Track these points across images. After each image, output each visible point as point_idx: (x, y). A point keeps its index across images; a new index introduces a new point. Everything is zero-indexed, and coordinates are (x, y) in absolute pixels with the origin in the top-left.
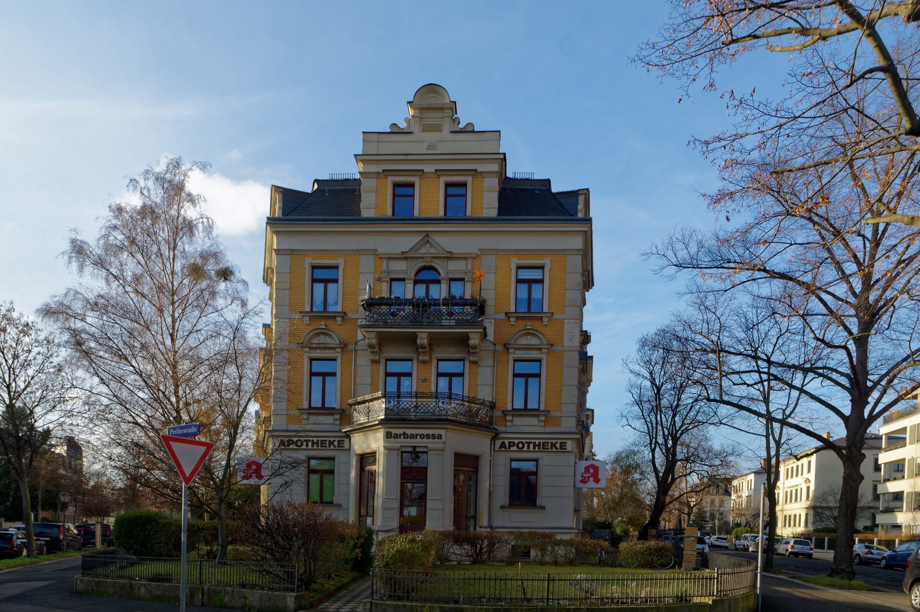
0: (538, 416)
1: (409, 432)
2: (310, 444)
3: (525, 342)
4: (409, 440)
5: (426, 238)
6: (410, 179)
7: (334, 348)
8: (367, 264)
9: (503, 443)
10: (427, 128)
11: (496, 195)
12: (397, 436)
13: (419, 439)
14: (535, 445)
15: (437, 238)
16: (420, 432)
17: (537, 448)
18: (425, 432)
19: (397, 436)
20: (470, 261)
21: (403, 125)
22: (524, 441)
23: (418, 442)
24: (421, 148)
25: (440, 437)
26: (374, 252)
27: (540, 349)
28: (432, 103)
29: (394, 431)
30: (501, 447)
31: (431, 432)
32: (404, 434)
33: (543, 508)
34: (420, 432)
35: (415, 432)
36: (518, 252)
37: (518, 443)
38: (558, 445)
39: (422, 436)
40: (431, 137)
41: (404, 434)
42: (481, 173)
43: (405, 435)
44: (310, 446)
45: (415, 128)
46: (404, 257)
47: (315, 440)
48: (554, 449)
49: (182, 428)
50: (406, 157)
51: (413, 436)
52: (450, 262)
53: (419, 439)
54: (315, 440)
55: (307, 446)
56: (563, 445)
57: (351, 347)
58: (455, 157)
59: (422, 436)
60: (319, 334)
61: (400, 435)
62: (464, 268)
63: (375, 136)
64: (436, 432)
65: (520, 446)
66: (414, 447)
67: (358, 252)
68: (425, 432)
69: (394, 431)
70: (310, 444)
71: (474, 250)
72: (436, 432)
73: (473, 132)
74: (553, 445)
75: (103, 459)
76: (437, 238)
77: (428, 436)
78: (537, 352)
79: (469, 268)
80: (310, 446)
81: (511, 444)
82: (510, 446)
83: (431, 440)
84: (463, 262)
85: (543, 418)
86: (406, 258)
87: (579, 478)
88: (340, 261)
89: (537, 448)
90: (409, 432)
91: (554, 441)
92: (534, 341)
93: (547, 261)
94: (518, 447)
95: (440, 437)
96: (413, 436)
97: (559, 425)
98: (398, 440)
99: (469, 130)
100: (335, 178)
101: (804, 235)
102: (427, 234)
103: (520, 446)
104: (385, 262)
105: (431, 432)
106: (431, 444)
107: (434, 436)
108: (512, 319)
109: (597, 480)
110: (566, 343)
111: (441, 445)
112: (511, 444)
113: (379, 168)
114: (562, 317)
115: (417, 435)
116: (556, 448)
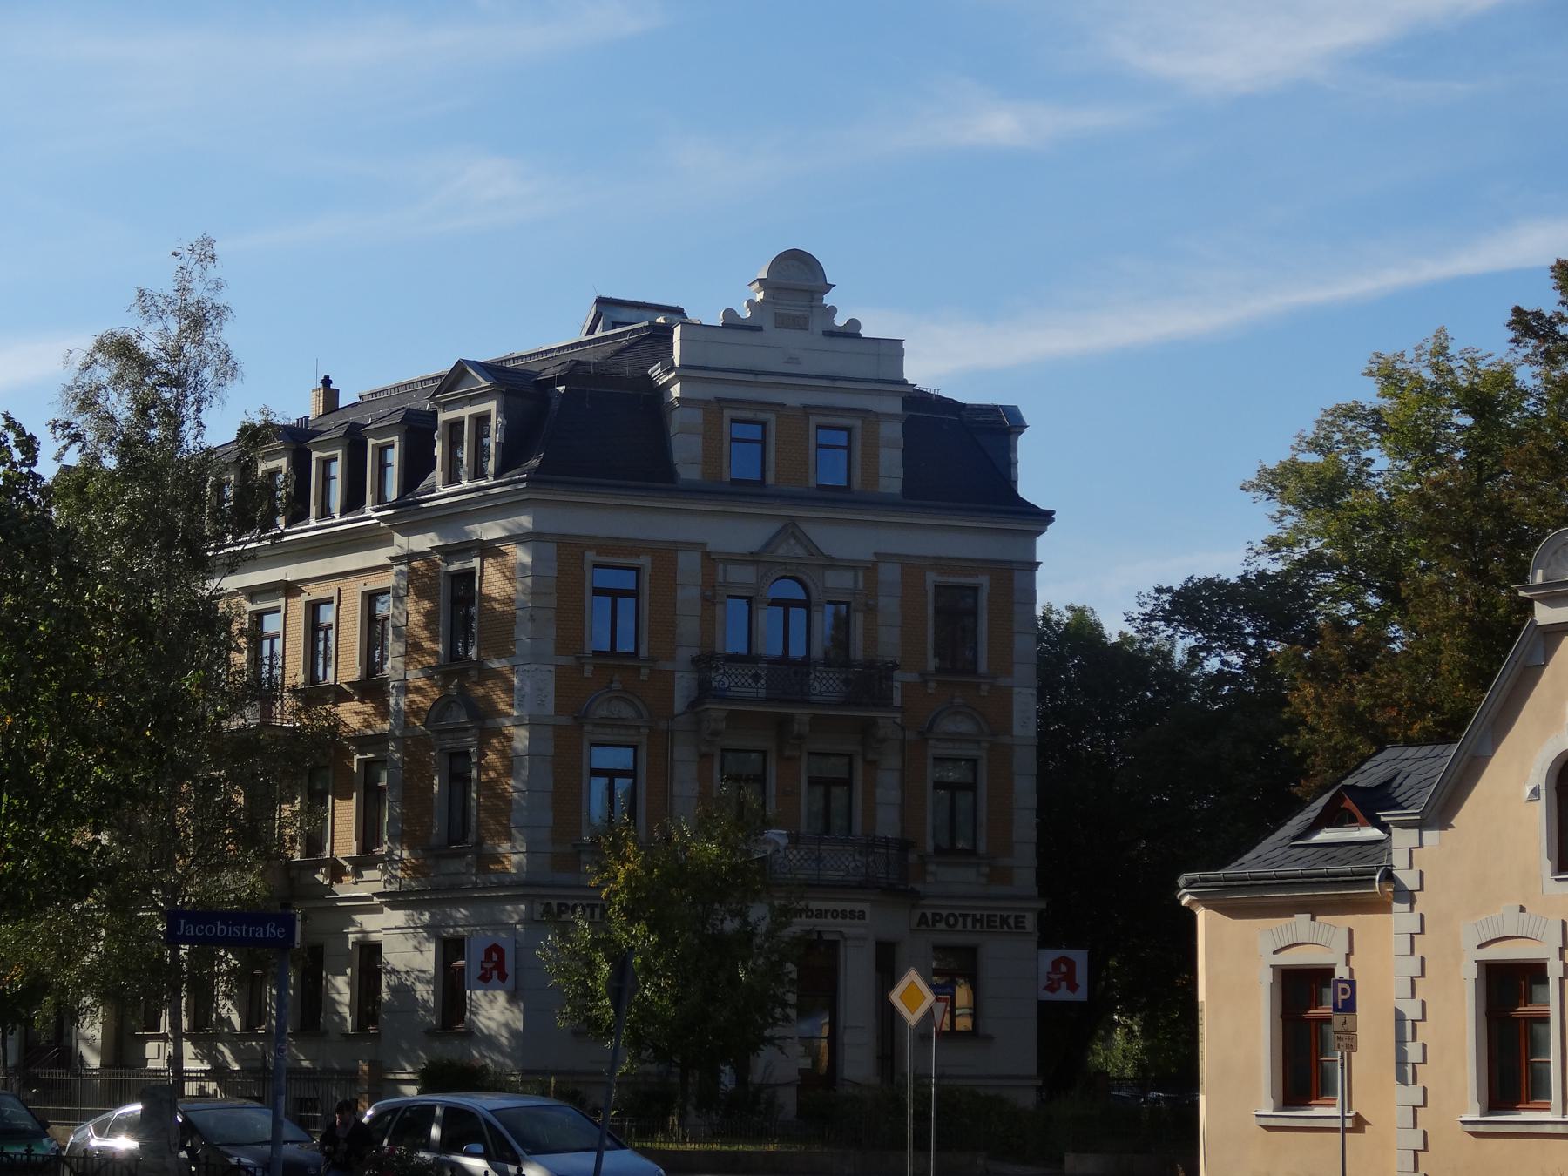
1: (815, 905)
2: (969, 921)
4: (814, 920)
5: (790, 529)
6: (762, 416)
9: (924, 915)
10: (784, 322)
11: (900, 452)
14: (975, 920)
16: (831, 905)
18: (840, 906)
21: (745, 314)
22: (957, 913)
25: (862, 915)
28: (796, 281)
31: (848, 906)
33: (989, 1038)
34: (831, 905)
35: (823, 905)
38: (1012, 921)
39: (835, 914)
45: (768, 324)
46: (753, 559)
49: (543, 896)
51: (821, 914)
55: (965, 925)
56: (1019, 920)
59: (835, 914)
64: (858, 907)
65: (952, 920)
67: (674, 547)
68: (840, 906)
70: (969, 921)
72: (858, 907)
73: (858, 336)
74: (1004, 921)
75: (433, 946)
77: (844, 914)
81: (937, 917)
82: (935, 922)
84: (849, 575)
85: (985, 870)
86: (756, 562)
87: (1044, 982)
91: (1005, 914)
94: (948, 924)
95: (862, 915)
96: (821, 914)
99: (851, 332)
103: (952, 920)
105: (848, 906)
108: (932, 685)
110: (1017, 730)
112: (937, 917)
116: (1009, 926)
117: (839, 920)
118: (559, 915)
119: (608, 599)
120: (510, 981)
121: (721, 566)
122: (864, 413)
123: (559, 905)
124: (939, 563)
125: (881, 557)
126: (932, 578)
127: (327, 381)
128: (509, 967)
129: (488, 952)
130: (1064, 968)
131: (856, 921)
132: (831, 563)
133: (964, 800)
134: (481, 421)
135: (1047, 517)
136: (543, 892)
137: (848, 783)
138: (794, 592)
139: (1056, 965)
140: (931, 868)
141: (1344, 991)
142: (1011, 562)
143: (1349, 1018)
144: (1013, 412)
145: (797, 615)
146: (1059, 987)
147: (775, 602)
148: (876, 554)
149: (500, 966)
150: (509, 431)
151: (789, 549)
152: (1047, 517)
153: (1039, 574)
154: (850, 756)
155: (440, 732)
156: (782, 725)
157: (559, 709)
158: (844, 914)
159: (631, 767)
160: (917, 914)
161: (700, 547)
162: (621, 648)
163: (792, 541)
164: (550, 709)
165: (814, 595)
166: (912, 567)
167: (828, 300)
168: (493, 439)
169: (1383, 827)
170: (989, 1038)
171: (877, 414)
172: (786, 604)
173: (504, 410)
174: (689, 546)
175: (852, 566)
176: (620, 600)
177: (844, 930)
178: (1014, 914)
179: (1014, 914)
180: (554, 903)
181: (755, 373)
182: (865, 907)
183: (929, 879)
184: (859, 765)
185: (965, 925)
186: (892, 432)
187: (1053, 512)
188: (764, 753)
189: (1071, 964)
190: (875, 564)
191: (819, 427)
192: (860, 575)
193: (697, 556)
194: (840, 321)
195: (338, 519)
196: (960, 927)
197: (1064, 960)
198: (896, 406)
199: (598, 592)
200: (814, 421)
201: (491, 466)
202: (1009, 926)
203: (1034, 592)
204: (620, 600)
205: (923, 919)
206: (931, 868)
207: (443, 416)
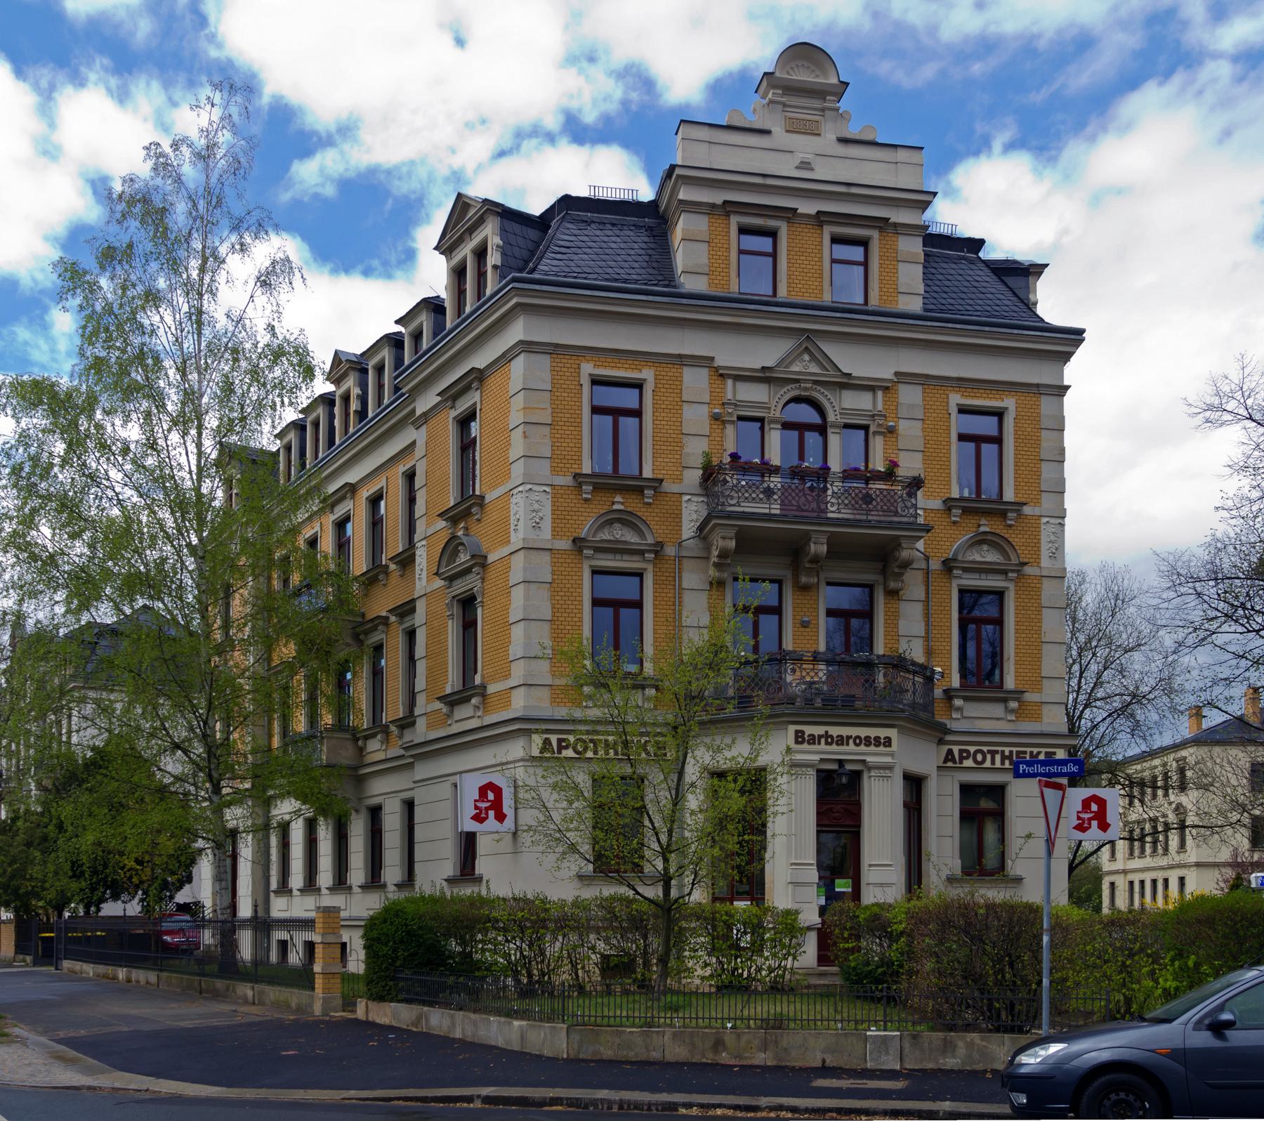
2: (998, 757)
3: (978, 558)
4: (834, 747)
6: (772, 223)
7: (642, 553)
8: (695, 381)
9: (950, 752)
12: (813, 740)
13: (852, 747)
18: (863, 732)
19: (813, 740)
20: (880, 394)
22: (985, 749)
23: (849, 751)
24: (785, 167)
25: (888, 742)
26: (704, 361)
27: (1005, 572)
31: (872, 732)
32: (827, 735)
36: (962, 383)
37: (977, 752)
39: (858, 741)
40: (804, 146)
41: (827, 735)
42: (895, 225)
44: (998, 764)
46: (765, 377)
50: (765, 182)
51: (841, 741)
53: (852, 747)
54: (1007, 750)
55: (993, 762)
57: (670, 551)
58: (848, 190)
59: (858, 741)
60: (610, 522)
61: (820, 737)
63: (704, 133)
65: (979, 757)
66: (841, 762)
67: (682, 360)
69: (809, 730)
70: (998, 757)
71: (887, 373)
72: (882, 733)
77: (868, 741)
79: (880, 406)
80: (998, 764)
82: (962, 759)
83: (872, 748)
88: (647, 374)
89: (1007, 765)
90: (835, 731)
91: (1035, 750)
92: (630, 537)
93: (1009, 403)
94: (975, 761)
95: (888, 742)
96: (841, 741)
97: (1038, 718)
98: (815, 747)
100: (603, 195)
102: (809, 335)
103: (979, 757)
104: (730, 382)
105: (872, 732)
106: (874, 756)
109: (1104, 826)
111: (888, 759)
112: (964, 755)
113: (717, 197)
114: (1037, 511)
115: (849, 737)
117: (863, 748)
122: (882, 224)
123: (961, 751)
125: (903, 378)
128: (507, 807)
129: (483, 791)
130: (1094, 807)
131: (882, 748)
132: (847, 383)
135: (1075, 336)
136: (544, 727)
138: (806, 414)
139: (1086, 804)
140: (958, 702)
144: (1053, 160)
145: (812, 438)
147: (787, 426)
149: (497, 806)
151: (804, 366)
152: (1075, 336)
153: (1068, 399)
157: (556, 534)
158: (868, 741)
159: (775, 603)
162: (623, 470)
163: (806, 357)
164: (546, 532)
165: (831, 417)
172: (801, 428)
173: (503, 232)
175: (870, 387)
177: (869, 759)
179: (1044, 750)
180: (554, 739)
181: (764, 176)
182: (892, 733)
185: (993, 762)
187: (1080, 332)
188: (779, 582)
189: (1102, 803)
196: (988, 764)
197: (1095, 798)
199: (596, 410)
205: (949, 756)
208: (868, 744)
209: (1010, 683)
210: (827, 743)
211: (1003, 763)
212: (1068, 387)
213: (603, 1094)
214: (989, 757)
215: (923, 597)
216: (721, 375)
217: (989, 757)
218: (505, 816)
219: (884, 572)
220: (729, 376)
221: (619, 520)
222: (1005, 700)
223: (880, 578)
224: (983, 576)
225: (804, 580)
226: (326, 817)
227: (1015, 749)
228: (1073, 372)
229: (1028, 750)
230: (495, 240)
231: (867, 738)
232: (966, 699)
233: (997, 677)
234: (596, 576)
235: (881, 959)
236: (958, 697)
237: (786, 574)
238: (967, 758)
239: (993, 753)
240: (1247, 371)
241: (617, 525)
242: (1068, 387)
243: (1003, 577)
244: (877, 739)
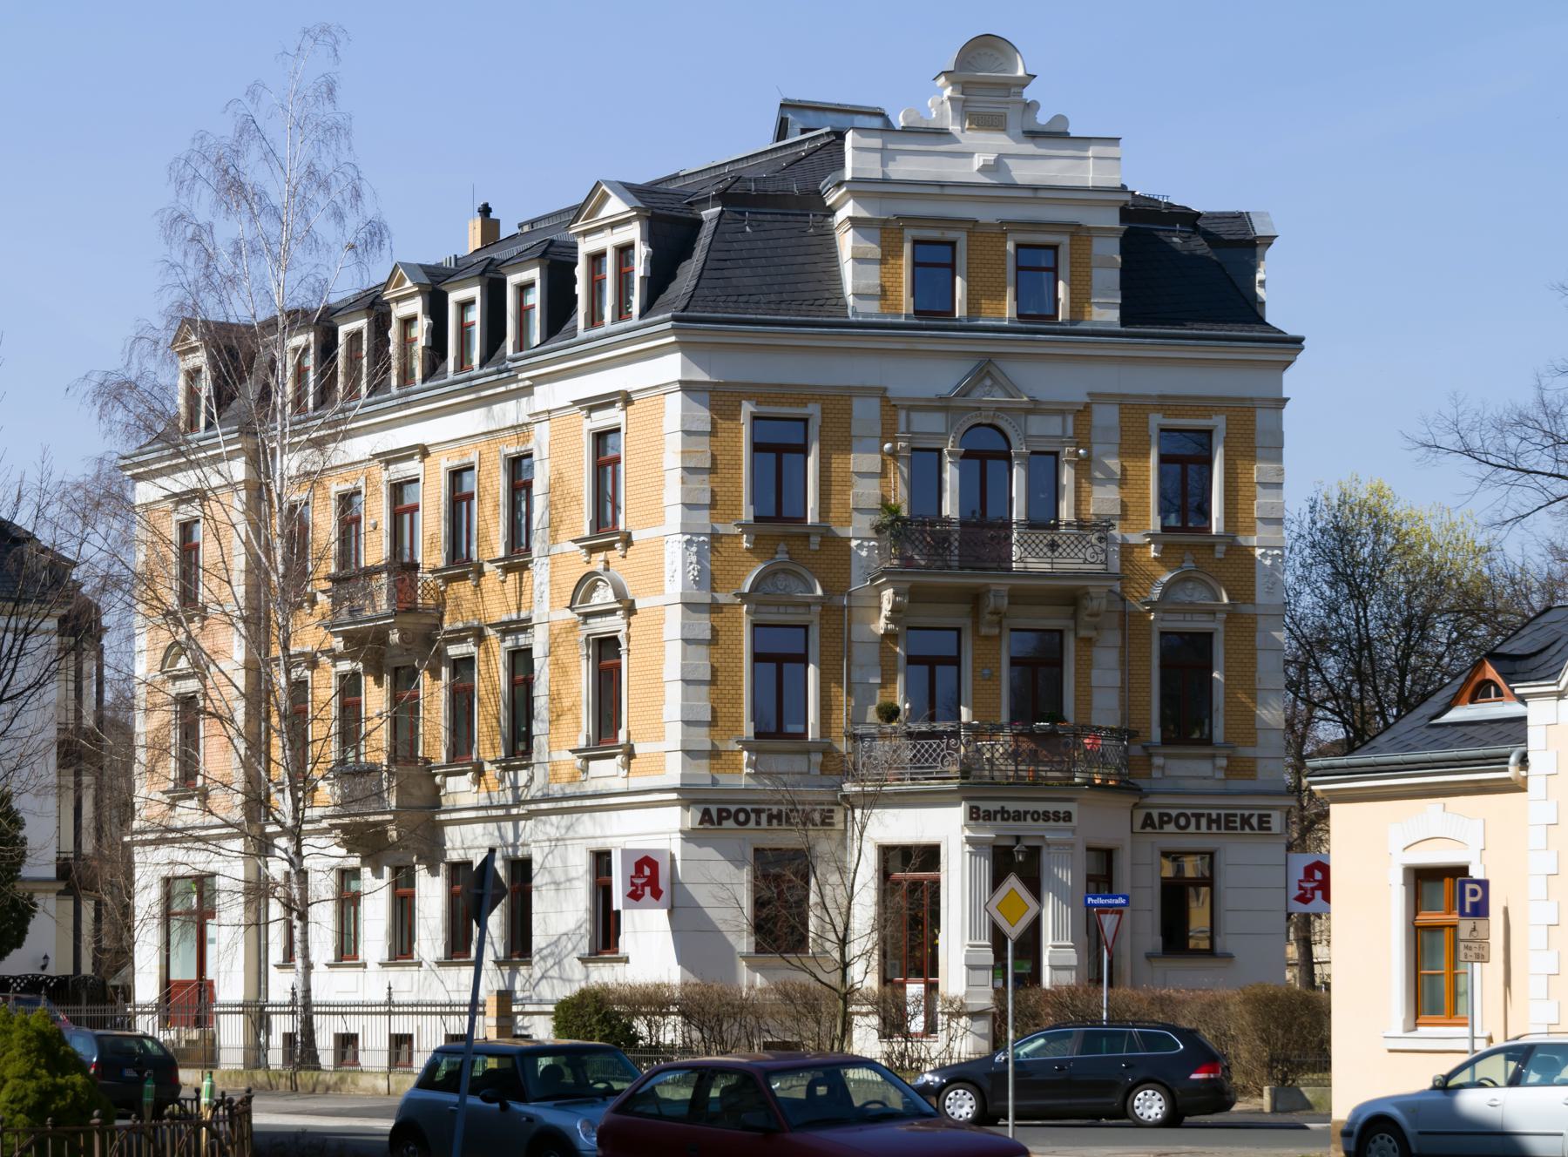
0: (1213, 757)
1: (1011, 807)
2: (1204, 822)
4: (1011, 822)
5: (985, 368)
6: (950, 235)
9: (1149, 816)
12: (989, 816)
14: (1210, 821)
15: (1014, 370)
17: (1214, 826)
22: (1189, 812)
23: (1028, 828)
25: (1068, 817)
29: (984, 806)
30: (1143, 827)
33: (1229, 957)
38: (1254, 821)
39: (1036, 816)
43: (1004, 814)
46: (941, 405)
47: (1214, 814)
48: (1247, 830)
51: (1018, 816)
52: (1032, 419)
54: (1214, 814)
55: (1198, 827)
56: (1264, 821)
59: (1036, 816)
61: (996, 812)
62: (1059, 432)
64: (1062, 807)
65: (1182, 821)
67: (846, 395)
68: (1041, 807)
69: (984, 806)
70: (1204, 822)
74: (1246, 821)
76: (1014, 370)
77: (1046, 816)
78: (1206, 618)
81: (1165, 819)
83: (1052, 823)
84: (1058, 420)
89: (1214, 826)
91: (1247, 813)
94: (737, 822)
95: (1068, 817)
96: (1018, 816)
101: (280, 796)
103: (1182, 821)
105: (1051, 807)
106: (1052, 833)
107: (1057, 816)
112: (1165, 819)
115: (1026, 813)
116: (1252, 828)
117: (1041, 822)
118: (720, 823)
119: (773, 456)
120: (665, 897)
121: (902, 415)
123: (1161, 815)
124: (1166, 404)
125: (1097, 397)
126: (1156, 420)
127: (485, 211)
128: (663, 884)
131: (1061, 823)
133: (944, 673)
134: (625, 250)
137: (956, 661)
141: (1474, 893)
142: (1251, 399)
143: (1480, 923)
146: (1312, 899)
148: (1089, 394)
149: (653, 882)
150: (654, 262)
153: (1288, 412)
154: (959, 630)
155: (587, 616)
156: (975, 598)
158: (1046, 816)
160: (1140, 816)
161: (882, 393)
166: (1133, 408)
167: (1029, 94)
168: (639, 269)
169: (1522, 699)
170: (1229, 957)
171: (1089, 229)
173: (651, 237)
174: (866, 391)
175: (1060, 411)
176: (990, 463)
178: (1257, 812)
179: (1257, 812)
180: (713, 809)
183: (1156, 774)
184: (1070, 644)
185: (1198, 827)
186: (1109, 251)
188: (959, 630)
190: (1087, 406)
191: (1018, 246)
192: (1070, 419)
193: (875, 404)
194: (1043, 118)
195: (477, 371)
196: (1192, 829)
198: (1111, 219)
200: (909, 234)
201: (635, 309)
202: (1252, 828)
203: (1282, 433)
204: (990, 463)
205: (1148, 821)
206: (1158, 761)
207: (586, 247)
208: (1047, 819)
209: (1219, 734)
210: (1003, 819)
211: (1209, 827)
212: (1287, 400)
213: (365, 347)
214: (1193, 821)
215: (1119, 643)
216: (890, 406)
217: (1193, 821)
218: (661, 892)
219: (1074, 617)
220: (903, 407)
221: (784, 571)
222: (1213, 757)
223: (1071, 623)
224: (1188, 617)
225: (984, 631)
226: (433, 871)
227: (1223, 812)
228: (1293, 381)
229: (1239, 812)
230: (641, 252)
231: (1046, 813)
232: (1166, 756)
233: (1206, 730)
234: (759, 665)
235: (29, 1112)
236: (1158, 755)
237: (965, 623)
238: (1168, 822)
239: (1198, 817)
240: (1461, 409)
241: (781, 576)
242: (1287, 400)
243: (1210, 618)
244: (1056, 813)
